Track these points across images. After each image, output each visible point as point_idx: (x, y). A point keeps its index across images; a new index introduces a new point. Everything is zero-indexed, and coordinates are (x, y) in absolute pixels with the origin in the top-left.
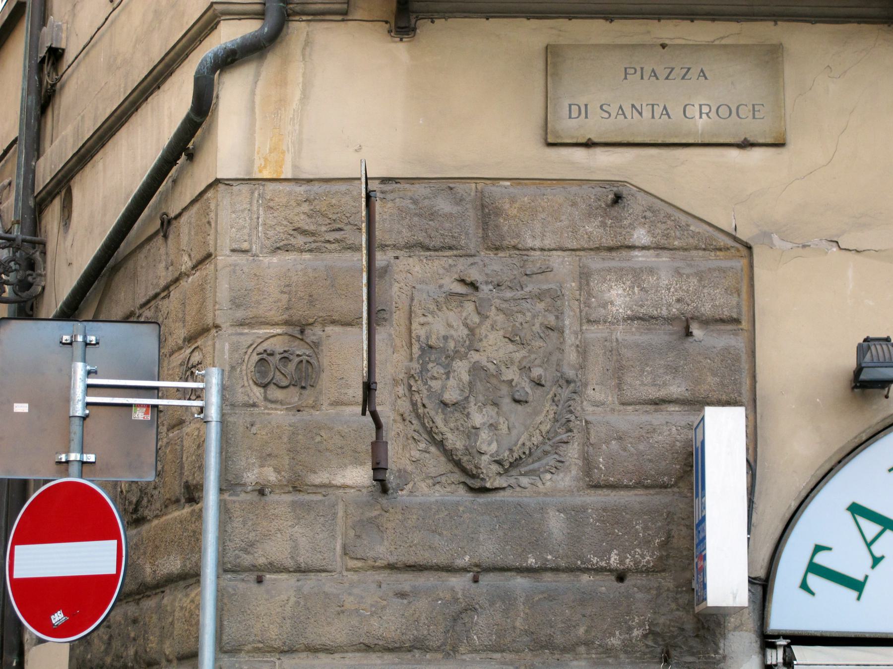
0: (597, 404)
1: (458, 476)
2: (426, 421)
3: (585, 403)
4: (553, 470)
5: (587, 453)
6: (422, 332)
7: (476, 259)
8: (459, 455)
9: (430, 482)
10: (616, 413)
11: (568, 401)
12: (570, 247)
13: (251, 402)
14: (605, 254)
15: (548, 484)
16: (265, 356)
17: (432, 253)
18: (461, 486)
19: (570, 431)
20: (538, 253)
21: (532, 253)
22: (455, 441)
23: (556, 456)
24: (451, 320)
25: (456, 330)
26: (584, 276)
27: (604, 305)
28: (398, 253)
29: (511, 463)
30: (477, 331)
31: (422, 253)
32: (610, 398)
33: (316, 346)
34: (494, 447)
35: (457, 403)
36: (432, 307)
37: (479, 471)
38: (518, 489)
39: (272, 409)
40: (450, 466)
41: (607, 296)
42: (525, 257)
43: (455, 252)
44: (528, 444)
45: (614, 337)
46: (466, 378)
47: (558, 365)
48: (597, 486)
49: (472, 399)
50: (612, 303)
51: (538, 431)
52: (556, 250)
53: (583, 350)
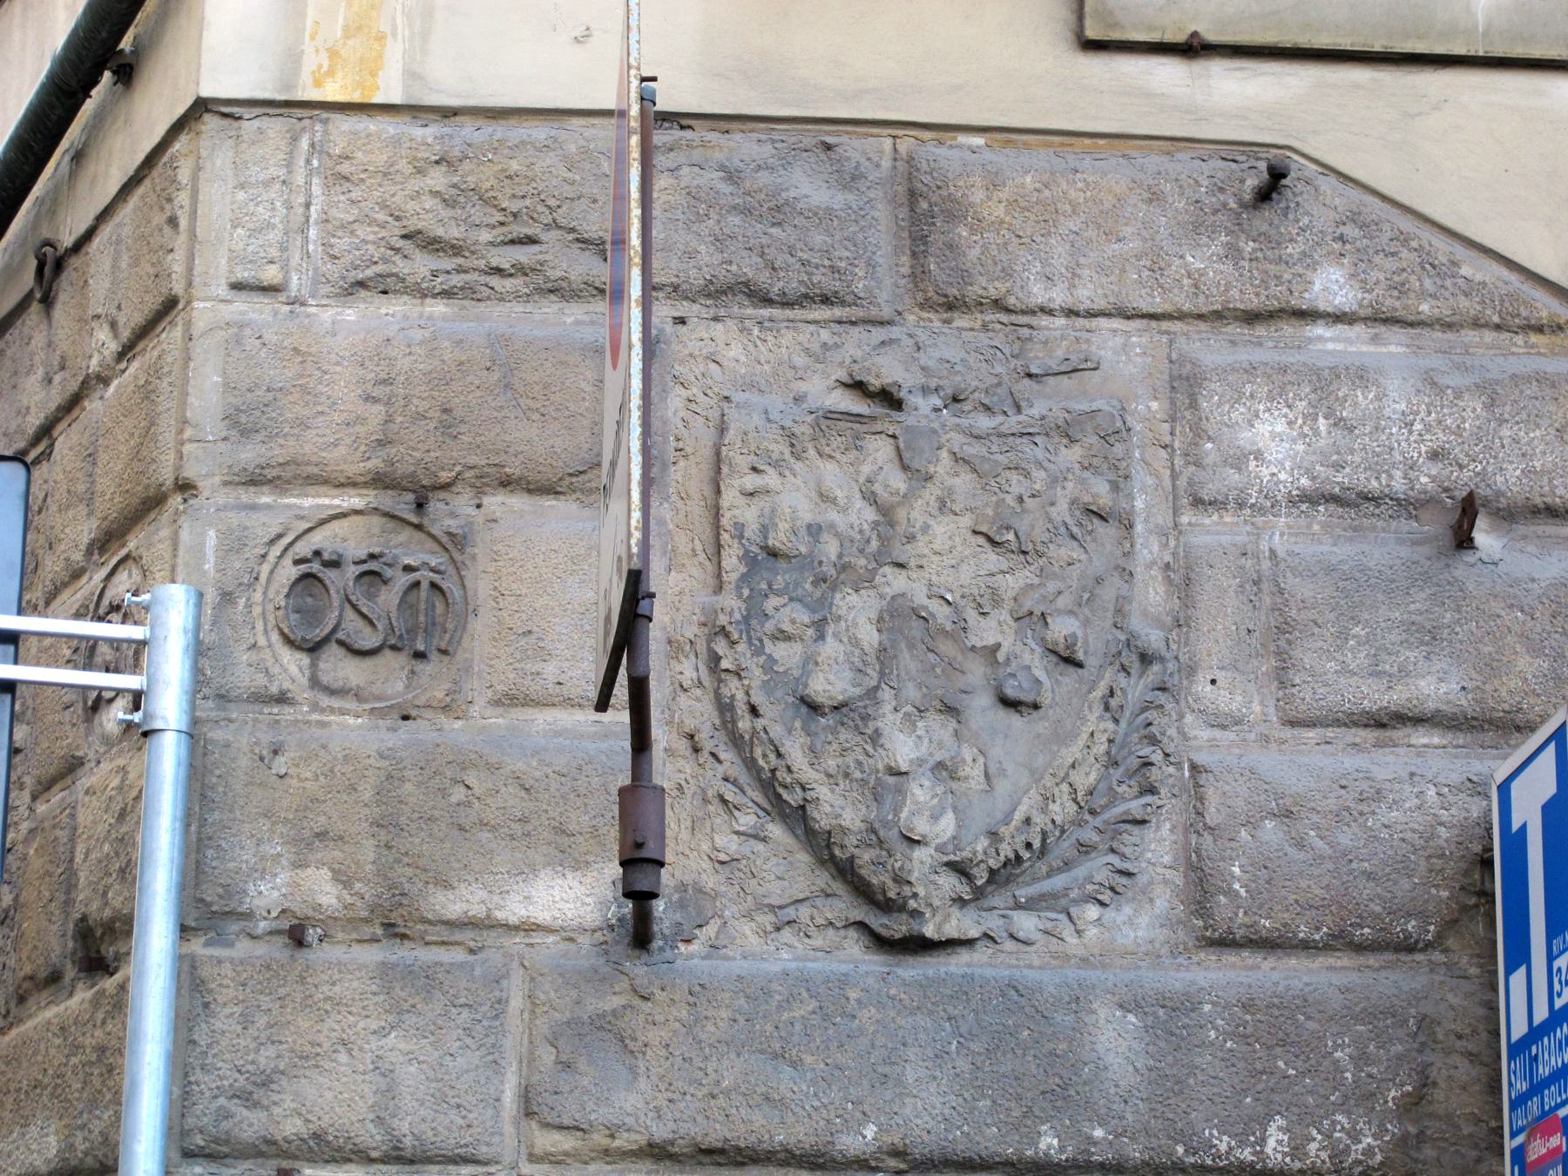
2: (758, 752)
3: (1189, 718)
6: (749, 515)
7: (894, 332)
9: (767, 920)
10: (1273, 746)
11: (1144, 710)
13: (274, 689)
14: (1235, 329)
15: (1092, 932)
16: (315, 567)
17: (776, 312)
18: (853, 933)
19: (1152, 791)
20: (1061, 321)
21: (1044, 321)
22: (839, 809)
26: (1184, 385)
27: (1238, 460)
28: (684, 308)
30: (901, 514)
31: (749, 311)
32: (1257, 708)
33: (456, 543)
35: (844, 705)
36: (780, 449)
37: (907, 890)
38: (1009, 945)
39: (332, 710)
40: (823, 878)
41: (1245, 437)
42: (1025, 332)
43: (838, 312)
44: (1039, 820)
45: (1264, 546)
46: (869, 636)
48: (1225, 943)
49: (886, 694)
50: (1259, 455)
51: (1065, 787)
52: (1108, 315)
53: (1183, 580)
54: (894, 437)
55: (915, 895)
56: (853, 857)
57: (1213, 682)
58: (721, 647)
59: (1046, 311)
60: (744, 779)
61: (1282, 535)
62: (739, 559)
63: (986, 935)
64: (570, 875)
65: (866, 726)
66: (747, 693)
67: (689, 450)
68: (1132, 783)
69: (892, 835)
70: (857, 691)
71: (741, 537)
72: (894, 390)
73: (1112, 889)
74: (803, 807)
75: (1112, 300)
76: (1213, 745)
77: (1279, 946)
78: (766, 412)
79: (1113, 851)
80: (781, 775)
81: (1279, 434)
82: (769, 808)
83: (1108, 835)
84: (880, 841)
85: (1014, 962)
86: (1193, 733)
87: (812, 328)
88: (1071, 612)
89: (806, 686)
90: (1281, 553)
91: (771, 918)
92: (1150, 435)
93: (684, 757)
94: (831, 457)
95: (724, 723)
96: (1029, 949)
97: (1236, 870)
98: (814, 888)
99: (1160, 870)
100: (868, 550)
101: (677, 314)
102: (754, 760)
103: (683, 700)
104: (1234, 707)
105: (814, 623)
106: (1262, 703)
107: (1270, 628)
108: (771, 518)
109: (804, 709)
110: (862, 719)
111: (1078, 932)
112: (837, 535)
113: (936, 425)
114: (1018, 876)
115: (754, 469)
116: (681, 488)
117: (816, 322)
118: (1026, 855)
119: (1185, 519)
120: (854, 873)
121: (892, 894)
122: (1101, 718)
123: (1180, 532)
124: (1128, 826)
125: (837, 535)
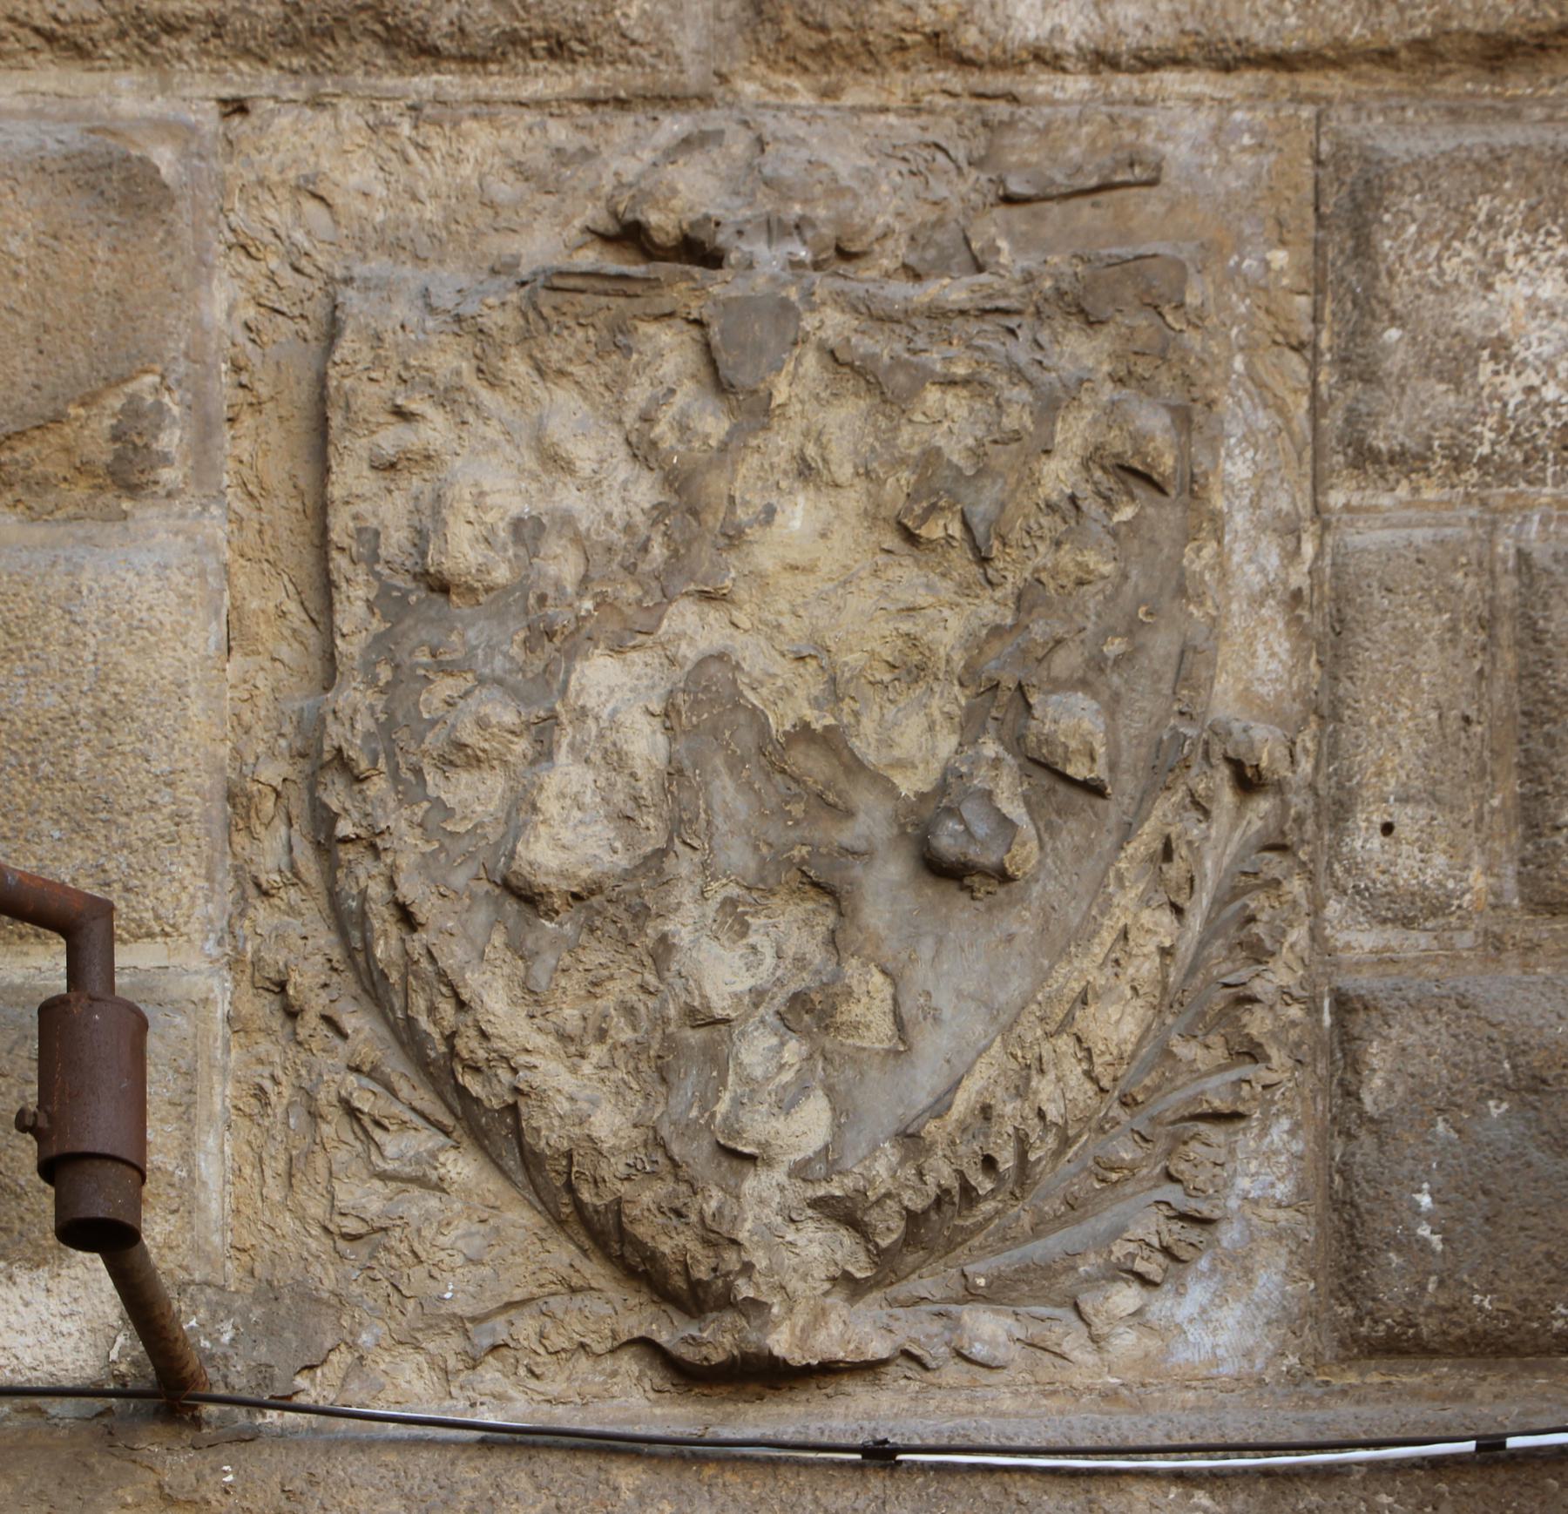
0: (1404, 909)
1: (626, 1312)
2: (420, 1003)
3: (1333, 908)
4: (1152, 1266)
5: (1345, 1170)
6: (391, 514)
7: (715, 119)
8: (612, 1182)
9: (449, 1347)
10: (1511, 957)
11: (1236, 893)
12: (1260, 35)
14: (1459, 84)
15: (1126, 1341)
17: (450, 82)
18: (628, 1364)
19: (1253, 1053)
20: (1077, 85)
21: (1043, 84)
22: (586, 1103)
23: (1172, 1193)
24: (558, 430)
25: (594, 485)
26: (1348, 210)
27: (1454, 362)
28: (242, 79)
29: (913, 1219)
30: (716, 484)
31: (389, 81)
32: (1477, 879)
34: (810, 1125)
35: (594, 888)
36: (450, 361)
37: (731, 1260)
38: (954, 1372)
40: (562, 1254)
41: (1470, 312)
42: (1001, 110)
43: (587, 78)
44: (1009, 1109)
45: (1505, 546)
46: (646, 745)
47: (1183, 677)
48: (1397, 1346)
49: (683, 865)
50: (1501, 349)
51: (1065, 1043)
52: (1179, 62)
53: (1329, 621)
54: (699, 323)
55: (748, 1268)
56: (619, 1201)
57: (1387, 829)
58: (335, 795)
59: (1048, 59)
60: (396, 1066)
61: (1545, 522)
62: (370, 605)
63: (907, 1354)
64: (23, 1277)
65: (641, 930)
66: (392, 884)
67: (264, 390)
68: (1214, 1039)
69: (696, 1154)
70: (623, 861)
71: (375, 557)
72: (702, 235)
73: (1166, 1250)
74: (513, 1109)
75: (1190, 25)
76: (1384, 959)
77: (1512, 1350)
78: (426, 293)
79: (1170, 1177)
80: (469, 1045)
81: (1549, 305)
82: (448, 1121)
83: (1161, 1146)
84: (675, 1165)
85: (963, 1406)
86: (1341, 938)
87: (530, 117)
88: (1083, 684)
89: (512, 855)
90: (1541, 556)
91: (456, 1341)
92: (1268, 323)
93: (268, 1032)
94: (561, 373)
95: (350, 953)
96: (994, 1378)
97: (1425, 1201)
98: (545, 1277)
99: (1267, 1213)
100: (644, 567)
101: (227, 92)
102: (410, 1021)
103: (262, 913)
104: (1428, 878)
105: (528, 725)
106: (1488, 870)
107: (1513, 716)
108: (436, 512)
109: (511, 906)
110: (635, 917)
111: (1094, 1339)
112: (578, 539)
113: (793, 294)
114: (972, 1232)
115: (401, 414)
116: (246, 472)
117: (539, 104)
118: (984, 1185)
119: (1336, 499)
120: (623, 1235)
121: (702, 1273)
122: (1144, 902)
123: (1326, 526)
124: (1203, 1127)
125: (578, 539)
